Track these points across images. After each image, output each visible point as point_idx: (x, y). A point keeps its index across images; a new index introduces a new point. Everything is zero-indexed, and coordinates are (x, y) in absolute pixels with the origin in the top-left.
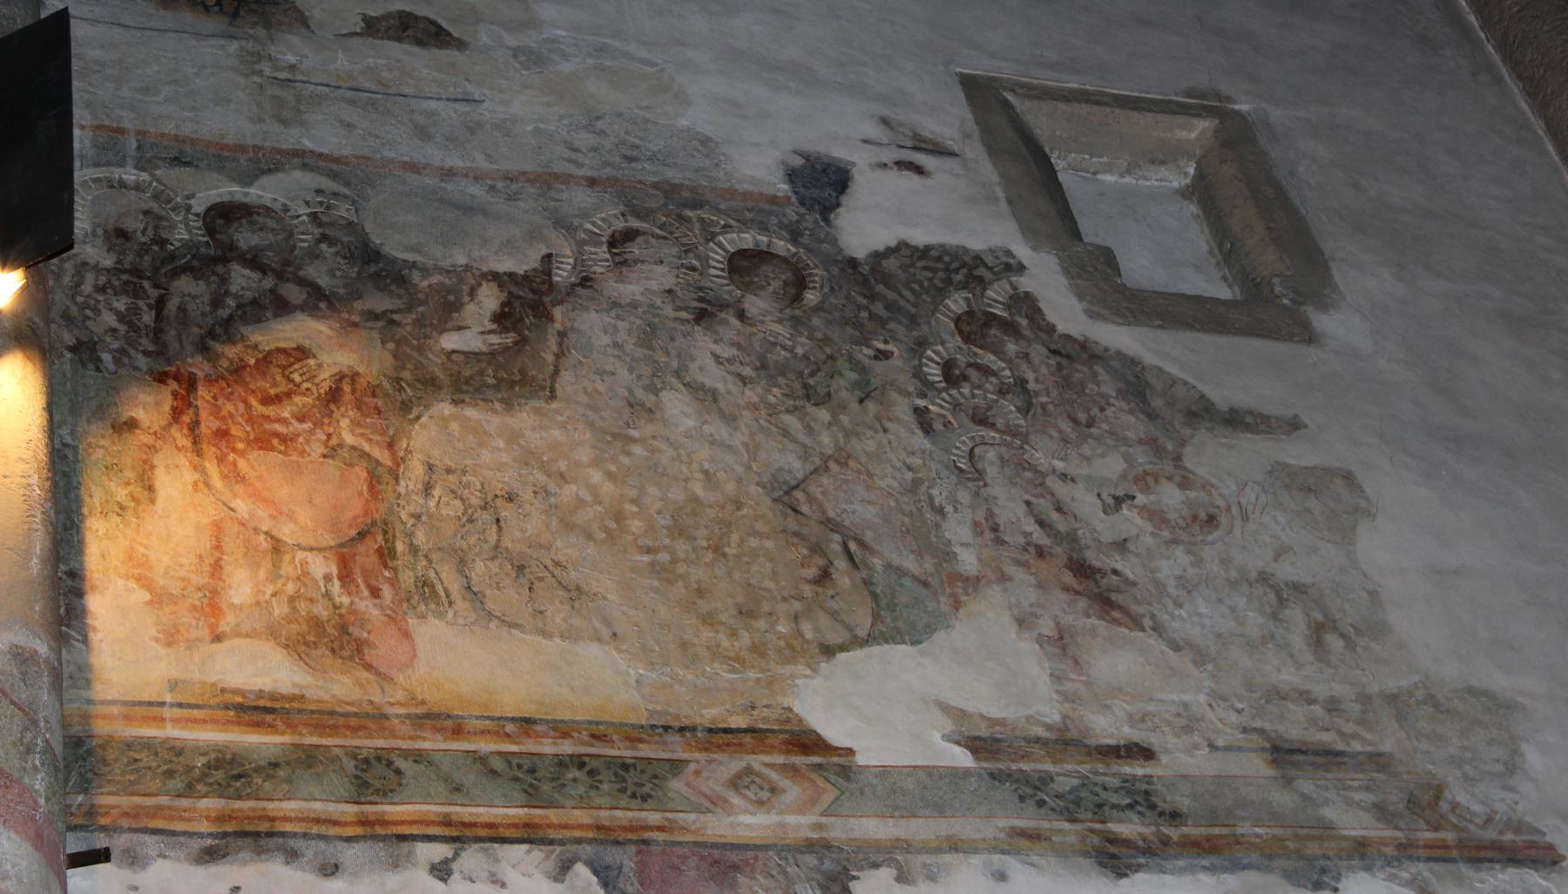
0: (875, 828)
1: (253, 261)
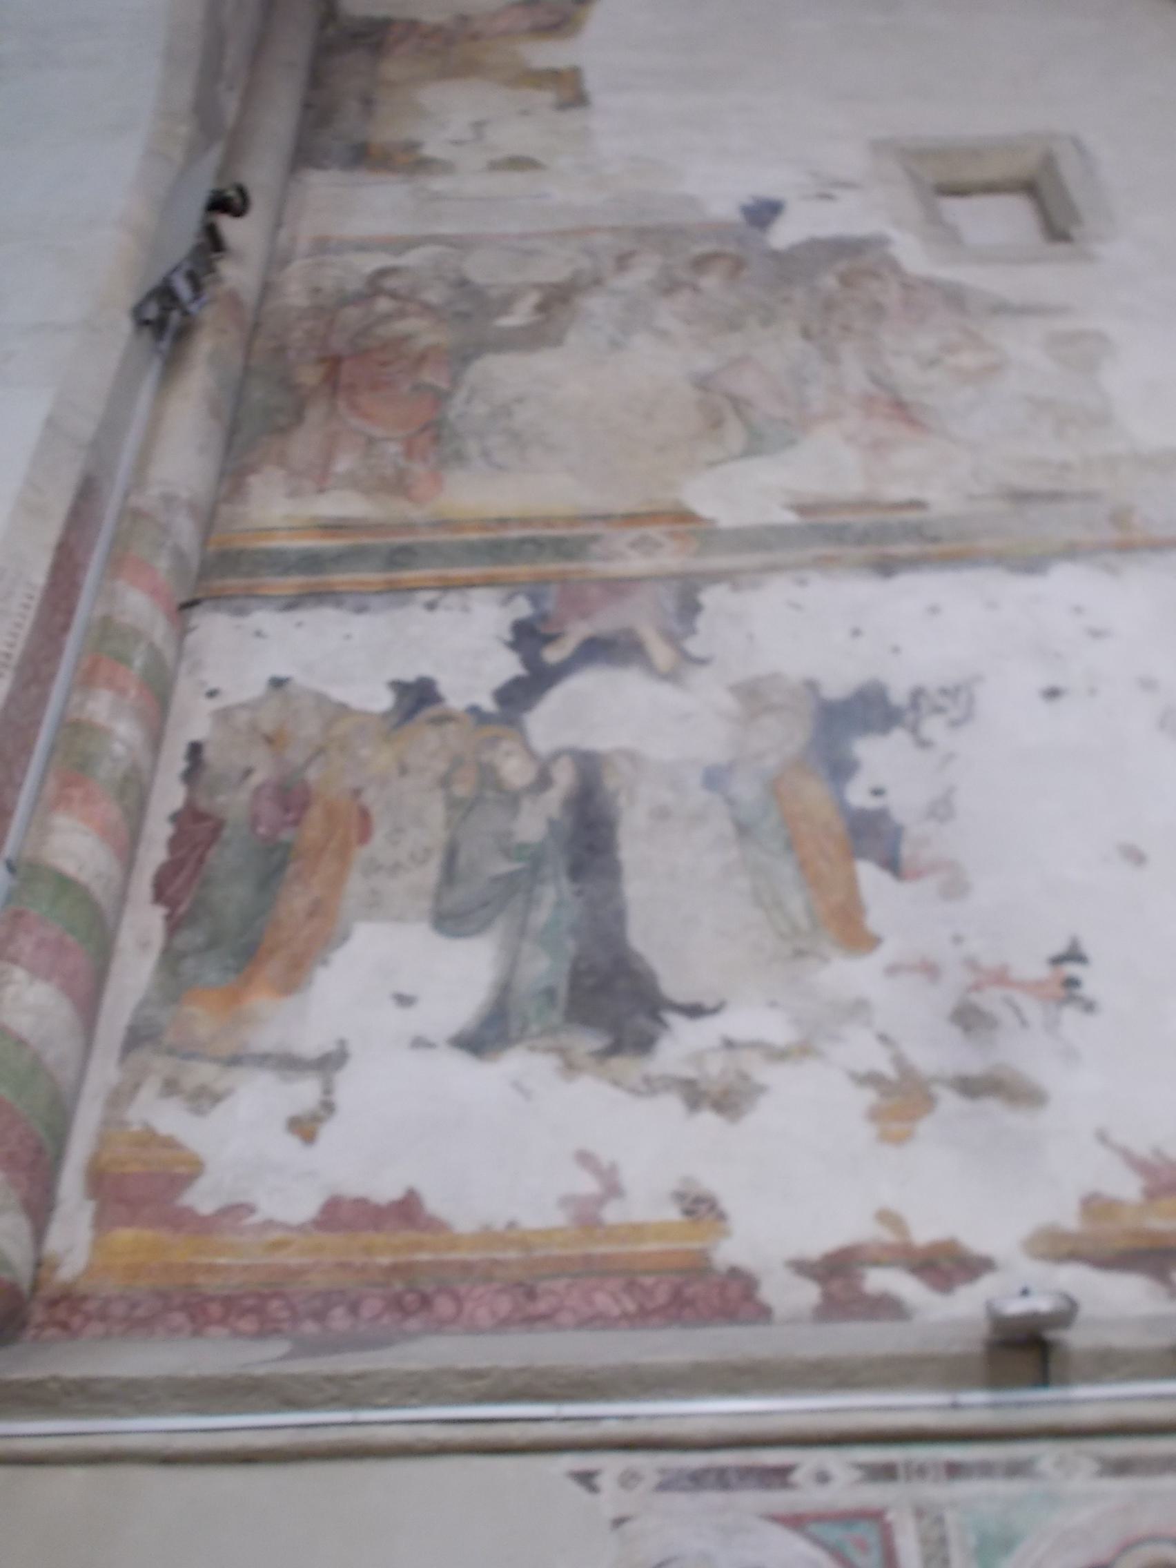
0: (718, 562)
1: (393, 295)
